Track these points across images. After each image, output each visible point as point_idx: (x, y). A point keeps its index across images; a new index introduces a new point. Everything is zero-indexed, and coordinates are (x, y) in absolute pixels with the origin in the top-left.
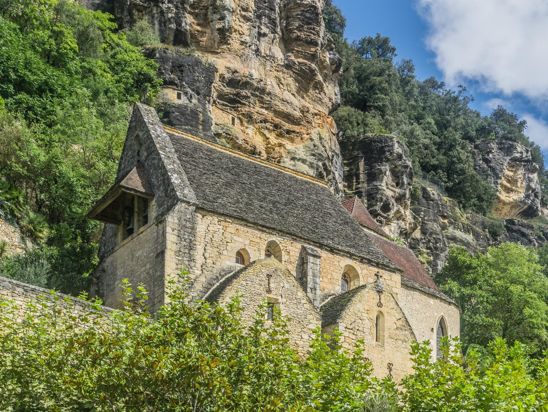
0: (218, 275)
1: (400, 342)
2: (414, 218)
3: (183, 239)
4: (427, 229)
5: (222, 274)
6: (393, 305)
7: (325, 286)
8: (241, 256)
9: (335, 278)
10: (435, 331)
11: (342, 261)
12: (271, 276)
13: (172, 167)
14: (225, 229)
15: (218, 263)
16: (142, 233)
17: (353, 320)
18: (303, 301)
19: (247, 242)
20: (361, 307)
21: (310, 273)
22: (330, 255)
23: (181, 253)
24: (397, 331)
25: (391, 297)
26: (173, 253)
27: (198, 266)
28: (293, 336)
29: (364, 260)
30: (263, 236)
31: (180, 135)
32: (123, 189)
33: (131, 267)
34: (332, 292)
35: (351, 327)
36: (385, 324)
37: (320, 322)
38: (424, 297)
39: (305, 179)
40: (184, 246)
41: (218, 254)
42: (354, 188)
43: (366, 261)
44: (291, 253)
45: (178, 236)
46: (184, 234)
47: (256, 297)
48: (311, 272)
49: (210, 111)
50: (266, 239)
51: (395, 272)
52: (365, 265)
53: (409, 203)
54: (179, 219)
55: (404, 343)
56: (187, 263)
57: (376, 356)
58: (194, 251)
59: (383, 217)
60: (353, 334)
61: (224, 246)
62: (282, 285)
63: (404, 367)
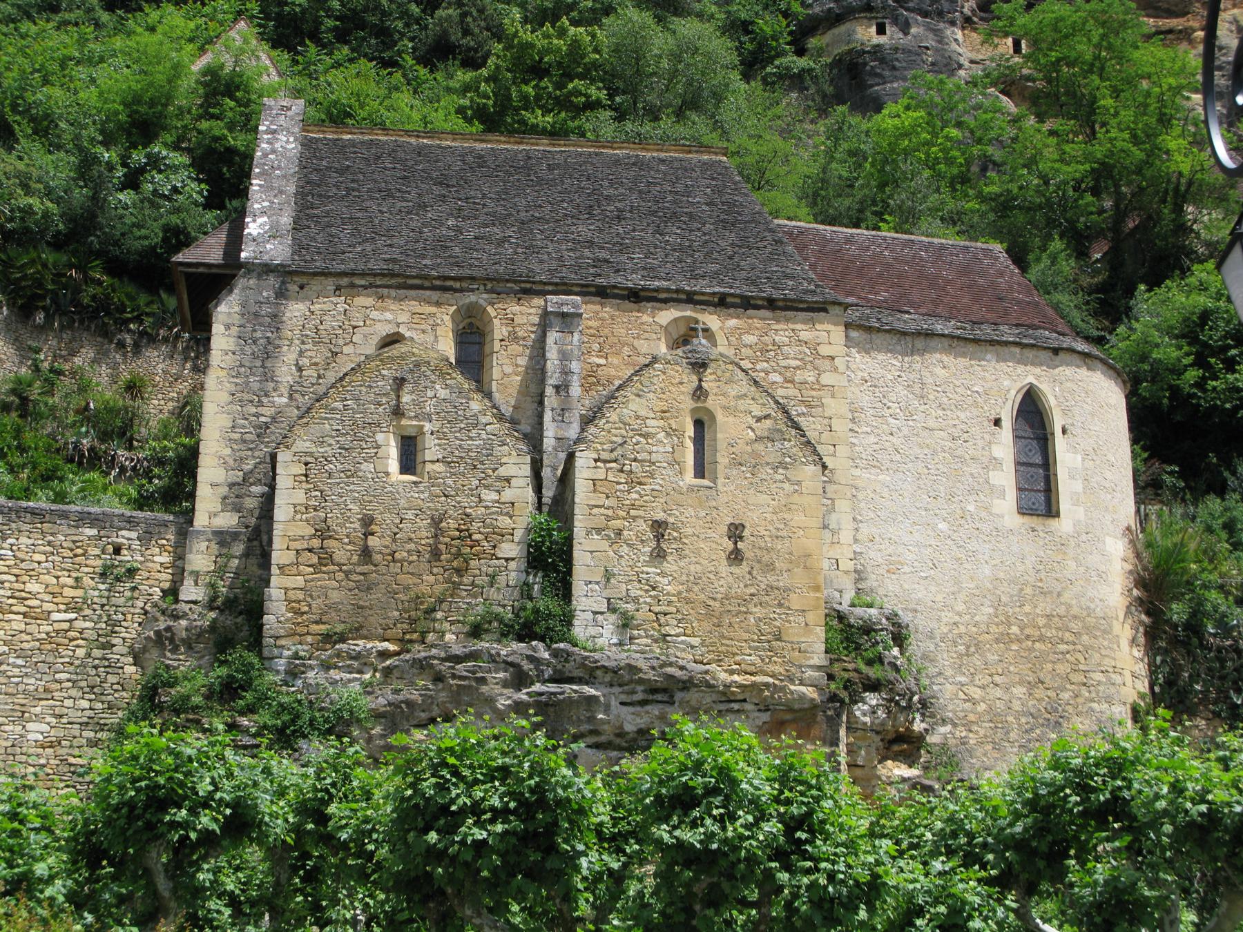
10: (1007, 424)
13: (266, 204)
18: (488, 419)
19: (404, 318)
28: (458, 499)
35: (613, 456)
36: (719, 436)
37: (529, 458)
44: (518, 320)
46: (255, 331)
49: (956, 40)
60: (622, 471)
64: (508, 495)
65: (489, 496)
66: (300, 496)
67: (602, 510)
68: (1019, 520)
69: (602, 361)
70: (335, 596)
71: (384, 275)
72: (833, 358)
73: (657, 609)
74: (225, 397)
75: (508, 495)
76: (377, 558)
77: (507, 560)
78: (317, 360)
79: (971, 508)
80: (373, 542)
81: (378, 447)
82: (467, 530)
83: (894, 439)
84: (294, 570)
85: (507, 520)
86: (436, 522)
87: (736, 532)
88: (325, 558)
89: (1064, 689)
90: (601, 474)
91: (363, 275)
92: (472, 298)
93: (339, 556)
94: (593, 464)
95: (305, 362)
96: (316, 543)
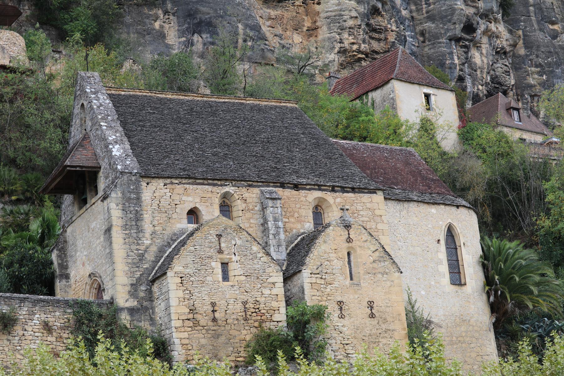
0: (170, 241)
1: (380, 276)
2: (510, 32)
3: (128, 212)
4: (531, 43)
5: (174, 238)
6: (365, 236)
7: (292, 226)
8: (193, 214)
9: (304, 214)
10: (443, 242)
11: (309, 195)
12: (221, 235)
13: (114, 137)
14: (172, 191)
15: (168, 229)
16: (94, 204)
17: (319, 264)
19: (198, 200)
20: (328, 250)
21: (270, 218)
22: (294, 192)
23: (127, 227)
24: (374, 264)
25: (363, 229)
26: (120, 228)
27: (147, 235)
29: (336, 188)
30: (215, 189)
31: (126, 93)
32: (68, 168)
33: (88, 239)
34: (302, 231)
35: (318, 271)
38: (426, 206)
39: (271, 104)
40: (131, 218)
41: (167, 219)
42: (424, 12)
43: (339, 189)
45: (123, 210)
46: (129, 207)
47: (207, 261)
48: (271, 217)
50: (218, 191)
51: (375, 193)
52: (337, 194)
53: (500, 16)
54: (123, 193)
55: (385, 276)
56: (135, 235)
57: (351, 297)
58: (142, 222)
59: (467, 40)
60: (321, 278)
61: (173, 209)
62: (234, 243)
63: (388, 302)
64: (275, 291)
65: (267, 292)
66: (180, 294)
67: (316, 297)
68: (453, 287)
69: (287, 220)
70: (203, 341)
71: (186, 178)
72: (381, 216)
73: (343, 342)
74: (121, 241)
75: (275, 291)
76: (220, 322)
77: (278, 322)
78: (161, 221)
79: (433, 283)
80: (217, 315)
81: (213, 269)
82: (258, 308)
83: (400, 252)
84: (183, 330)
85: (276, 303)
86: (245, 303)
87: (371, 305)
88: (196, 323)
89: (475, 364)
90: (314, 280)
91: (176, 178)
92: (227, 189)
93: (203, 322)
94: (310, 276)
95: (156, 223)
96: (191, 316)
